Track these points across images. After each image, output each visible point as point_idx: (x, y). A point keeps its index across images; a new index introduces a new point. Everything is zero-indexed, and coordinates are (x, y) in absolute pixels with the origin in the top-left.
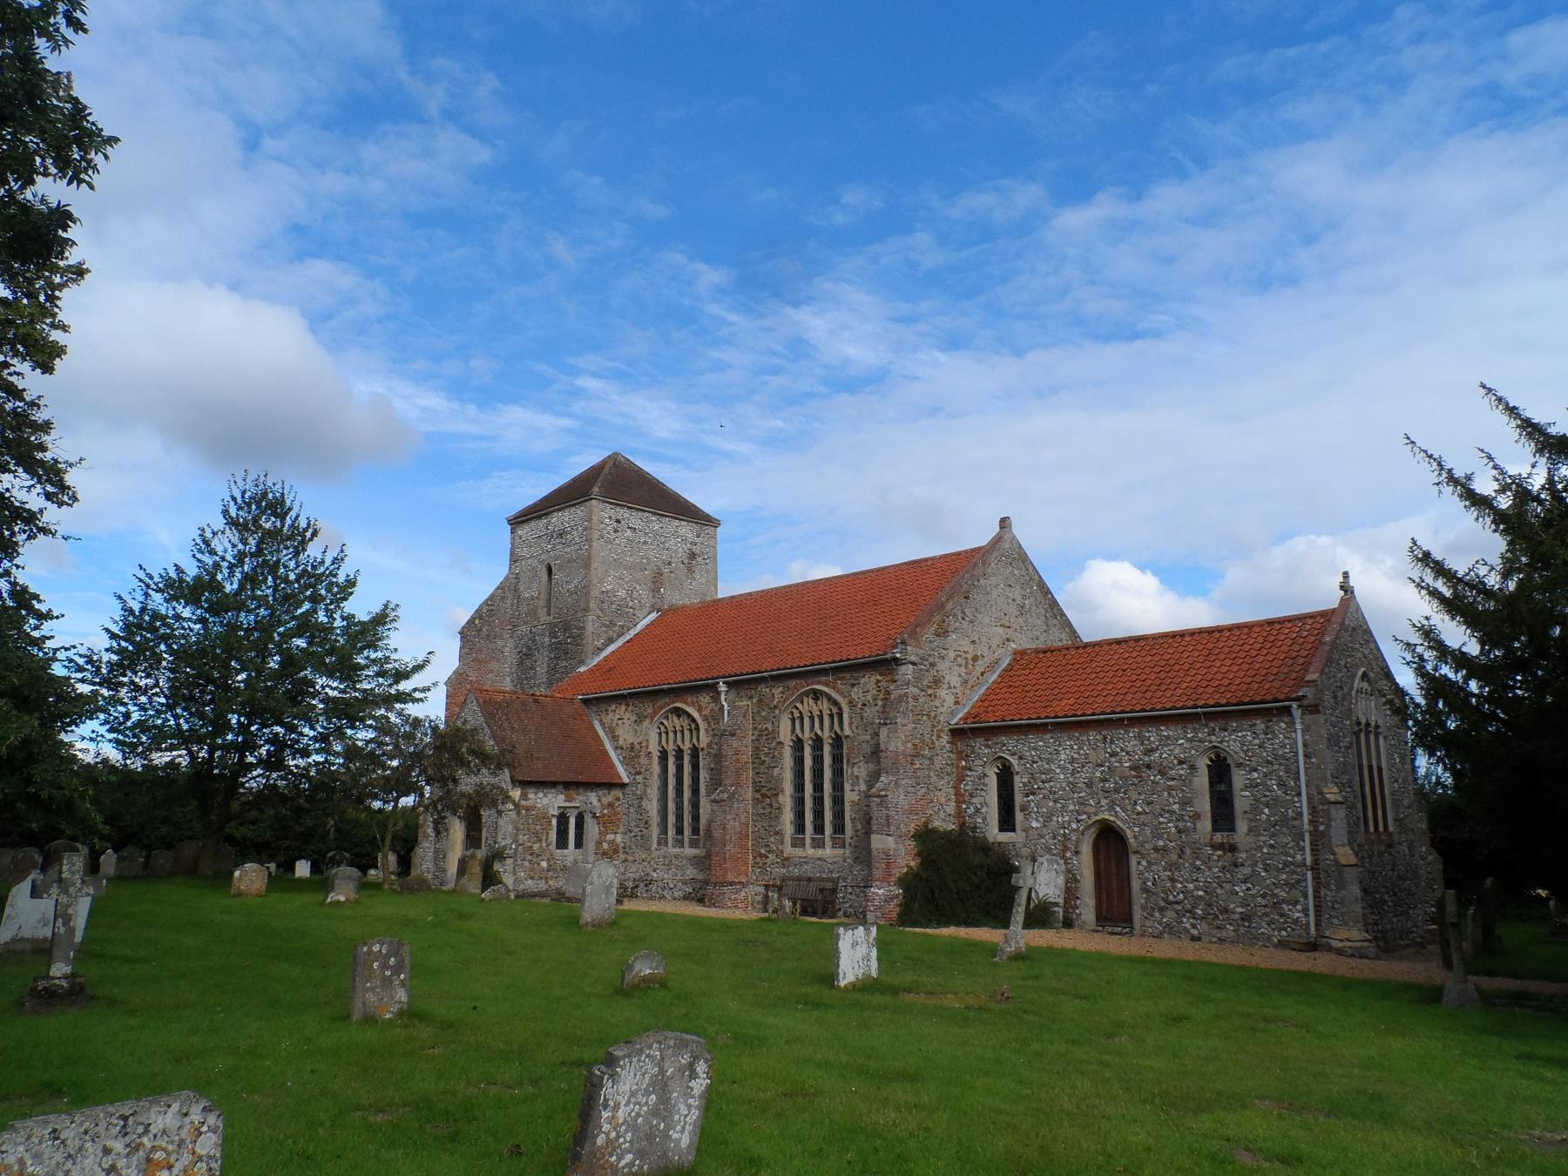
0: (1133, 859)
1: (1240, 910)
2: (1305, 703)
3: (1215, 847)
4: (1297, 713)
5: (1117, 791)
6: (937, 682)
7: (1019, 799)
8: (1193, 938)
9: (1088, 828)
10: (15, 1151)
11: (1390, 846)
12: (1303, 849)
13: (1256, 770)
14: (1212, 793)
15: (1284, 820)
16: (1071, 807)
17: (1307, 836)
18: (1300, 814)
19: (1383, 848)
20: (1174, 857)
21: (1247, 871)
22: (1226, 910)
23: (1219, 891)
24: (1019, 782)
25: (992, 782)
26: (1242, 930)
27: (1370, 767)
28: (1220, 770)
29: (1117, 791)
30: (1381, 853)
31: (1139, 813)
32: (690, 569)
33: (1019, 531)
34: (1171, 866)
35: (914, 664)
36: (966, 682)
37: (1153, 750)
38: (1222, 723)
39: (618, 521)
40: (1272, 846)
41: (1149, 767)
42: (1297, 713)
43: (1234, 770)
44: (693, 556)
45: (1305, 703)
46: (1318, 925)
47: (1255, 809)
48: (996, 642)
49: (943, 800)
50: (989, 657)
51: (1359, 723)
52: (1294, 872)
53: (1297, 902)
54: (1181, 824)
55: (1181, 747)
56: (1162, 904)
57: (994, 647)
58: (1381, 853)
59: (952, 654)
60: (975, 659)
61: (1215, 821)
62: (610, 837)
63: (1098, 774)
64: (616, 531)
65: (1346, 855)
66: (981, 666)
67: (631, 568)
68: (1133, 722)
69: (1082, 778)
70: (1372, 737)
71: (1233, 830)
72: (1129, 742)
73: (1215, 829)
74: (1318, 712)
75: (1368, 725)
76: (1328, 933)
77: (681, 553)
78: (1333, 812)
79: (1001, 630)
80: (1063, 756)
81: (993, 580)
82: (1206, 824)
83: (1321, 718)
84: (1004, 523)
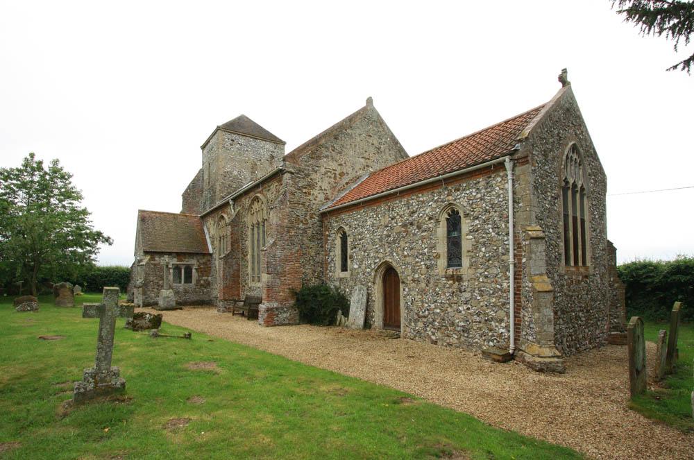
0: (401, 286)
1: (462, 324)
2: (516, 156)
3: (448, 278)
4: (508, 165)
5: (394, 242)
6: (311, 186)
7: (349, 251)
8: (435, 343)
9: (379, 267)
10: (690, 256)
11: (586, 277)
12: (508, 278)
13: (477, 218)
14: (449, 238)
15: (496, 256)
16: (372, 255)
17: (511, 267)
18: (508, 250)
19: (580, 278)
20: (423, 285)
21: (467, 295)
22: (453, 324)
23: (449, 310)
24: (349, 240)
25: (338, 242)
26: (463, 339)
27: (575, 219)
28: (454, 222)
29: (394, 242)
30: (579, 282)
31: (405, 256)
32: (271, 163)
33: (376, 105)
34: (423, 292)
35: (292, 173)
36: (335, 187)
37: (414, 212)
38: (456, 185)
39: (233, 140)
40: (486, 277)
41: (412, 224)
42: (508, 165)
43: (463, 220)
44: (272, 157)
45: (516, 156)
46: (516, 340)
47: (476, 247)
48: (358, 166)
49: (313, 254)
50: (352, 175)
51: (567, 183)
52: (501, 297)
53: (501, 321)
54: (428, 263)
55: (430, 206)
56: (416, 317)
57: (357, 169)
58: (579, 282)
59: (323, 170)
60: (342, 174)
61: (449, 259)
62: (205, 278)
63: (385, 232)
64: (231, 145)
65: (544, 284)
66: (346, 179)
67: (239, 162)
68: (403, 193)
69: (377, 236)
70: (578, 196)
71: (460, 265)
72: (400, 208)
73: (449, 265)
74: (527, 162)
75: (575, 185)
76: (523, 347)
77: (267, 155)
78: (534, 247)
79: (362, 160)
80: (369, 223)
81: (358, 131)
82: (442, 262)
83: (529, 168)
84: (370, 101)
